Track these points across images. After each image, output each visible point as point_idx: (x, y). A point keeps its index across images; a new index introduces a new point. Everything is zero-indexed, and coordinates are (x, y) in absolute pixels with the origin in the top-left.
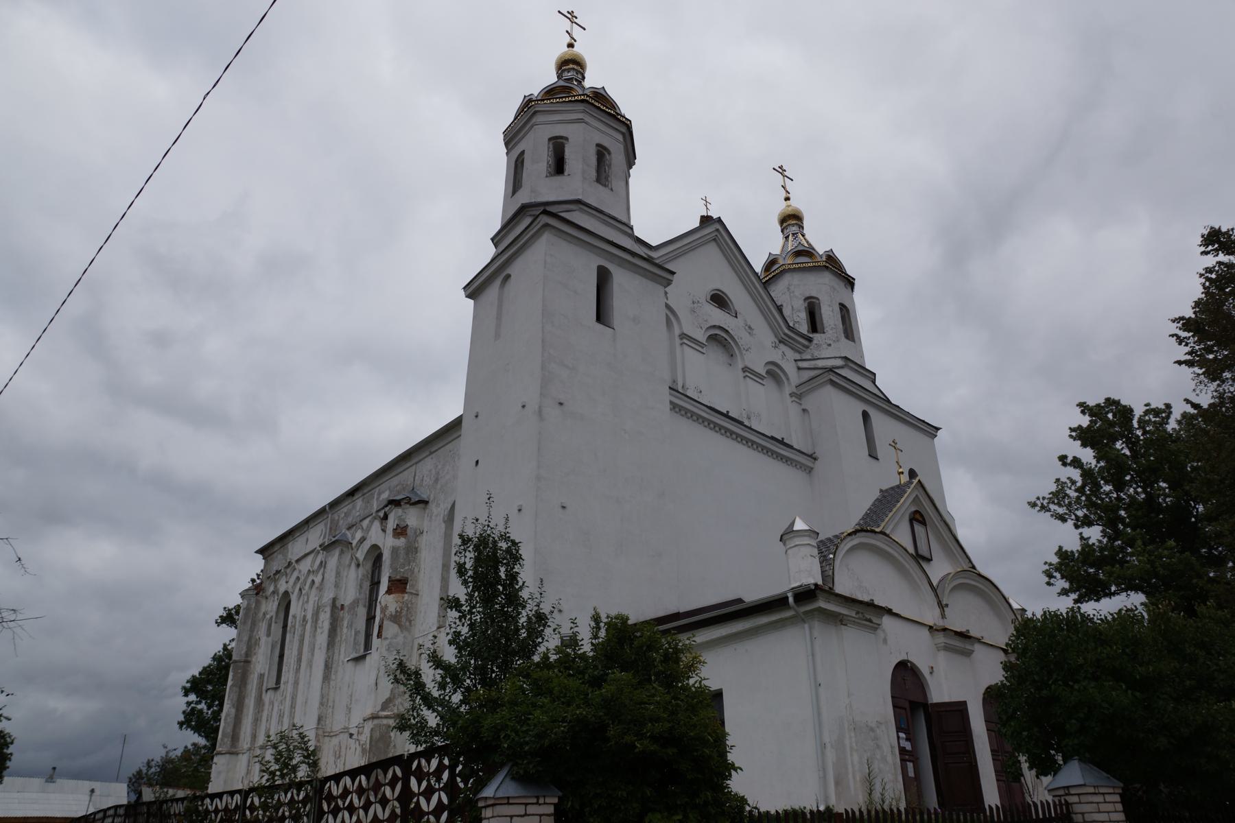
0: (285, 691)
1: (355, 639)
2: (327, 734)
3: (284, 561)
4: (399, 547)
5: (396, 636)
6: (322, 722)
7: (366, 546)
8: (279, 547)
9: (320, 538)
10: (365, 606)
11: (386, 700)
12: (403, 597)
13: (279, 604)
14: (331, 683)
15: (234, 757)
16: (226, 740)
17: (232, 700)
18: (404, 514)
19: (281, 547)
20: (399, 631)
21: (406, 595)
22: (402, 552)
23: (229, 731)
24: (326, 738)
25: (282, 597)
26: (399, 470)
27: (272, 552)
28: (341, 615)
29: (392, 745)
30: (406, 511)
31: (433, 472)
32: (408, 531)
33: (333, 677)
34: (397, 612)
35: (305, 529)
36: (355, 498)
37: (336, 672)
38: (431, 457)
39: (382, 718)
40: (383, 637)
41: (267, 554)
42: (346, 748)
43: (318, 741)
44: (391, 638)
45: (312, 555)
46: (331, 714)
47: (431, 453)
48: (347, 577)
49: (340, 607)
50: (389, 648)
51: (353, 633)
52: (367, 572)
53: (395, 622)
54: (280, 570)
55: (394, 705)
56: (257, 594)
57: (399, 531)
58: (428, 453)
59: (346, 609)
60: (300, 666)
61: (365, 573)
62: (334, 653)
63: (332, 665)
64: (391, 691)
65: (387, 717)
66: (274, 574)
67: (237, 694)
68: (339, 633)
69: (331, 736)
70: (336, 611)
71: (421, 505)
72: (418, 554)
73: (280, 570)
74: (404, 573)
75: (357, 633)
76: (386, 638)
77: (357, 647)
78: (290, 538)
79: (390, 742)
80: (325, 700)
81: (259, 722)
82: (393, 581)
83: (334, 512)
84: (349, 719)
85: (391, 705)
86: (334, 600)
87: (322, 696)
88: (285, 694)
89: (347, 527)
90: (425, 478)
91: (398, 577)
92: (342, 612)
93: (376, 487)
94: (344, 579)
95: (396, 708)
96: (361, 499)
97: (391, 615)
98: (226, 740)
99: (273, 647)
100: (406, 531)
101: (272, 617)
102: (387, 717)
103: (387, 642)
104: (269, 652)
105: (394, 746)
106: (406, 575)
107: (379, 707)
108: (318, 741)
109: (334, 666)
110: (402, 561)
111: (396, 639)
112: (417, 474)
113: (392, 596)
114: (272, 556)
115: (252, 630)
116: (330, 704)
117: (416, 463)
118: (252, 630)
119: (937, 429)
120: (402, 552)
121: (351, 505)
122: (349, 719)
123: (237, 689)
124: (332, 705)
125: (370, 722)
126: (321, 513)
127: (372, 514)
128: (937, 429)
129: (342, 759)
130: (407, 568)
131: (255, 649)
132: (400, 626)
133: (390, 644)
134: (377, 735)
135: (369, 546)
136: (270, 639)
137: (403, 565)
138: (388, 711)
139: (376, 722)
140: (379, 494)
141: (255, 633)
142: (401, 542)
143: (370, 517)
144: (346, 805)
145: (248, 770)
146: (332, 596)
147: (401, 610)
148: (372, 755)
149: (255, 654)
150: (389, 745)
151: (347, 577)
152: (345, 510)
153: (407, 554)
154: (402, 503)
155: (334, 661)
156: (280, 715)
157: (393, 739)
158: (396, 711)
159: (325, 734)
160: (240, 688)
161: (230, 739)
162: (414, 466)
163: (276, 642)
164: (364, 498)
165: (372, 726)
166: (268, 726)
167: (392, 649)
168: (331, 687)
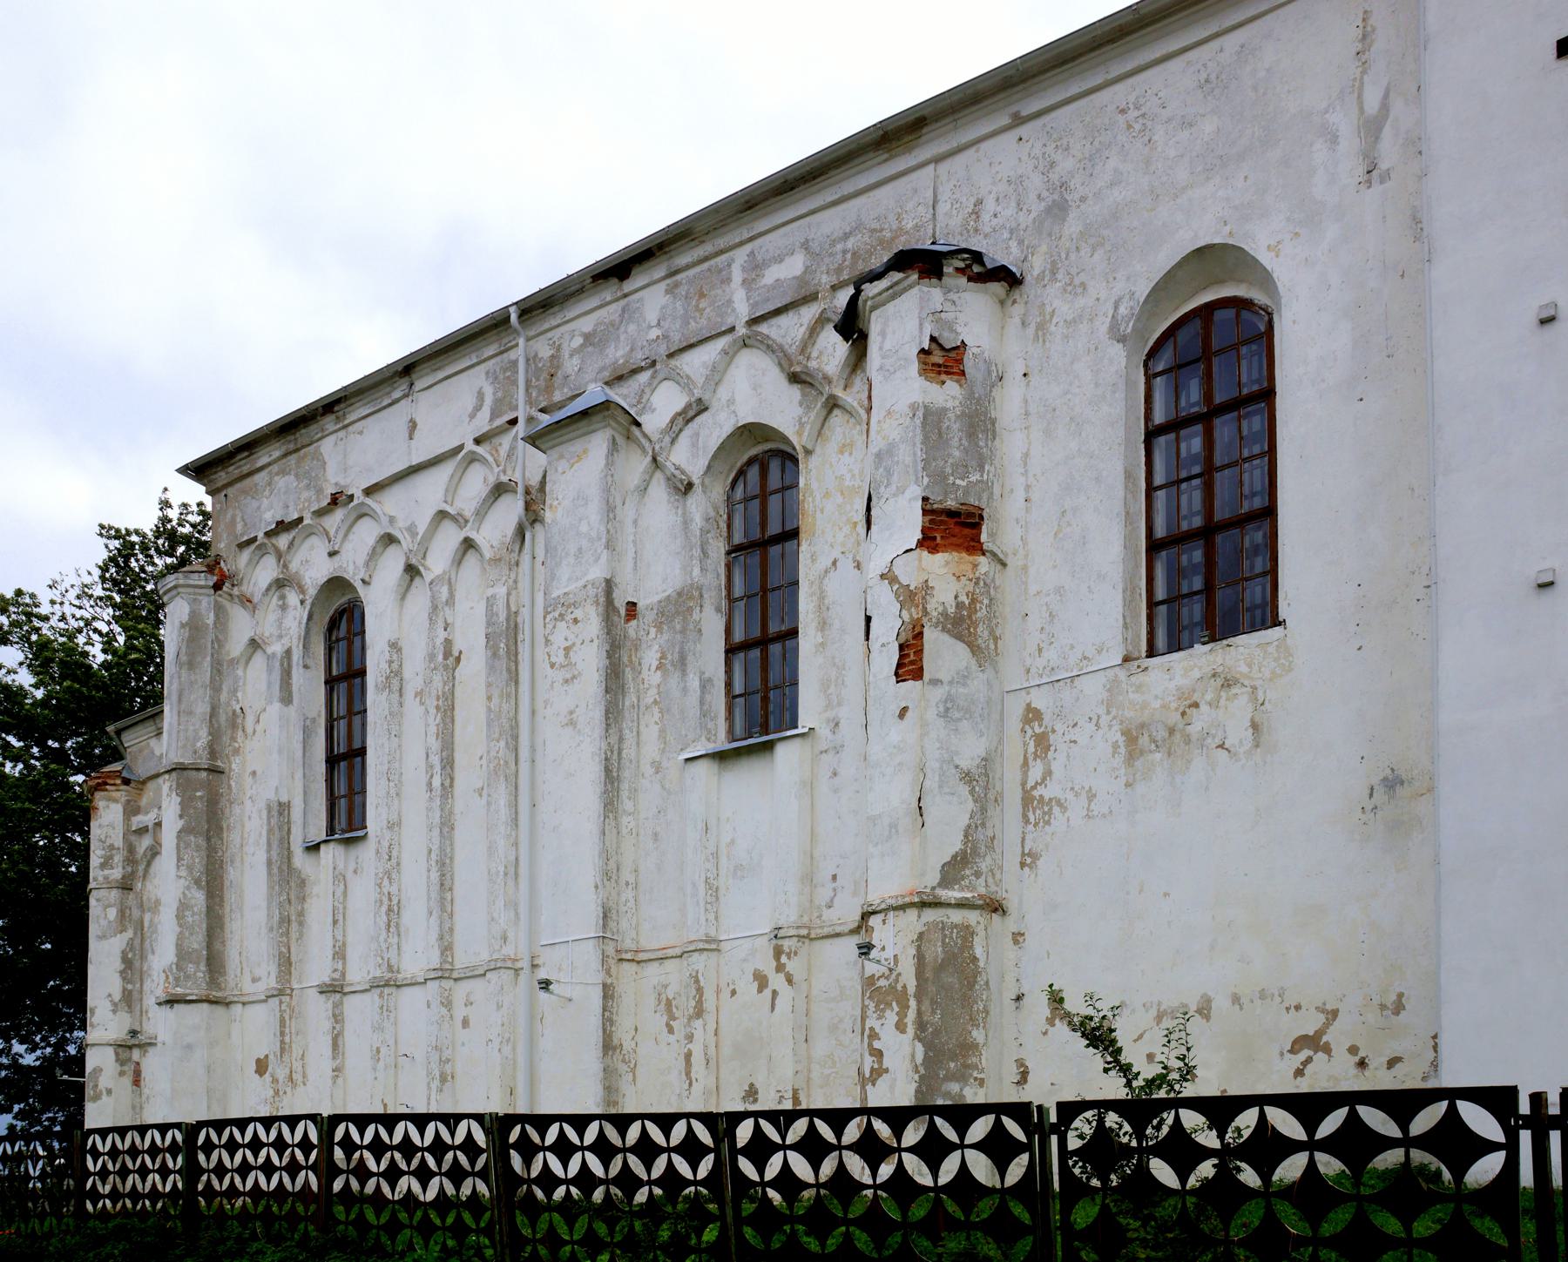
0: (396, 847)
1: (702, 703)
2: (629, 956)
3: (311, 493)
4: (945, 410)
5: (963, 678)
6: (612, 924)
7: (715, 429)
8: (276, 454)
9: (472, 416)
10: (718, 610)
11: (954, 857)
12: (975, 566)
13: (310, 618)
14: (625, 820)
15: (220, 1010)
16: (191, 968)
17: (190, 868)
18: (948, 306)
19: (285, 455)
20: (973, 662)
21: (982, 559)
22: (956, 426)
23: (196, 946)
24: (626, 965)
25: (317, 598)
26: (848, 187)
27: (246, 469)
28: (632, 633)
29: (981, 980)
30: (952, 296)
31: (1036, 182)
32: (969, 363)
33: (628, 805)
34: (959, 606)
35: (397, 394)
36: (628, 286)
37: (634, 791)
38: (1012, 135)
39: (949, 905)
40: (926, 676)
41: (222, 477)
42: (718, 992)
43: (608, 973)
44: (951, 683)
45: (446, 470)
46: (631, 904)
47: (1019, 120)
48: (635, 522)
49: (623, 612)
50: (947, 710)
51: (696, 684)
52: (716, 509)
53: (959, 637)
54: (300, 520)
55: (978, 874)
56: (217, 587)
57: (937, 358)
58: (1005, 120)
59: (647, 617)
60: (452, 779)
61: (712, 514)
62: (621, 740)
63: (619, 769)
64: (966, 836)
65: (962, 905)
66: (268, 534)
67: (204, 854)
68: (630, 685)
69: (638, 962)
70: (616, 618)
71: (998, 288)
72: (997, 442)
73: (300, 520)
74: (966, 491)
75: (705, 684)
76: (936, 682)
77: (710, 725)
78: (329, 423)
79: (976, 973)
80: (612, 864)
81: (294, 926)
82: (933, 512)
83: (532, 333)
84: (716, 918)
85: (968, 872)
86: (609, 585)
87: (605, 855)
88: (394, 854)
89: (606, 375)
90: (990, 205)
91: (951, 503)
92: (634, 623)
93: (742, 244)
94: (630, 529)
95: (982, 881)
96: (663, 286)
97: (945, 614)
98: (191, 968)
99: (307, 733)
100: (960, 361)
101: (288, 652)
102: (962, 905)
103: (938, 693)
104: (298, 747)
105: (987, 983)
106: (972, 500)
107: (933, 878)
108: (608, 973)
109: (626, 774)
110: (957, 453)
111: (964, 685)
112: (942, 197)
113: (940, 558)
114: (247, 482)
115: (216, 688)
116: (627, 875)
117: (938, 160)
118: (216, 688)
119: (898, 682)
120: (955, 430)
121: (613, 307)
122: (716, 918)
123: (202, 842)
124: (631, 880)
125: (912, 914)
126: (494, 327)
127: (732, 329)
128: (898, 682)
129: (710, 1019)
130: (974, 478)
131: (233, 739)
132: (974, 649)
133: (949, 698)
134: (935, 951)
135: (728, 429)
136: (292, 711)
137: (963, 469)
138: (962, 890)
139: (931, 915)
140: (755, 267)
141: (224, 696)
142: (948, 394)
143: (722, 343)
144: (310, 1162)
145: (282, 1042)
146: (597, 573)
147: (974, 601)
148: (926, 1006)
149: (237, 751)
150: (971, 986)
151: (635, 522)
152: (587, 324)
153: (972, 435)
154: (948, 270)
155: (625, 762)
156: (390, 910)
157: (981, 964)
158: (983, 891)
159: (624, 956)
160: (208, 839)
161: (203, 967)
162: (931, 167)
163: (314, 721)
164: (677, 285)
165: (920, 928)
166: (340, 938)
167: (957, 715)
168: (624, 831)
